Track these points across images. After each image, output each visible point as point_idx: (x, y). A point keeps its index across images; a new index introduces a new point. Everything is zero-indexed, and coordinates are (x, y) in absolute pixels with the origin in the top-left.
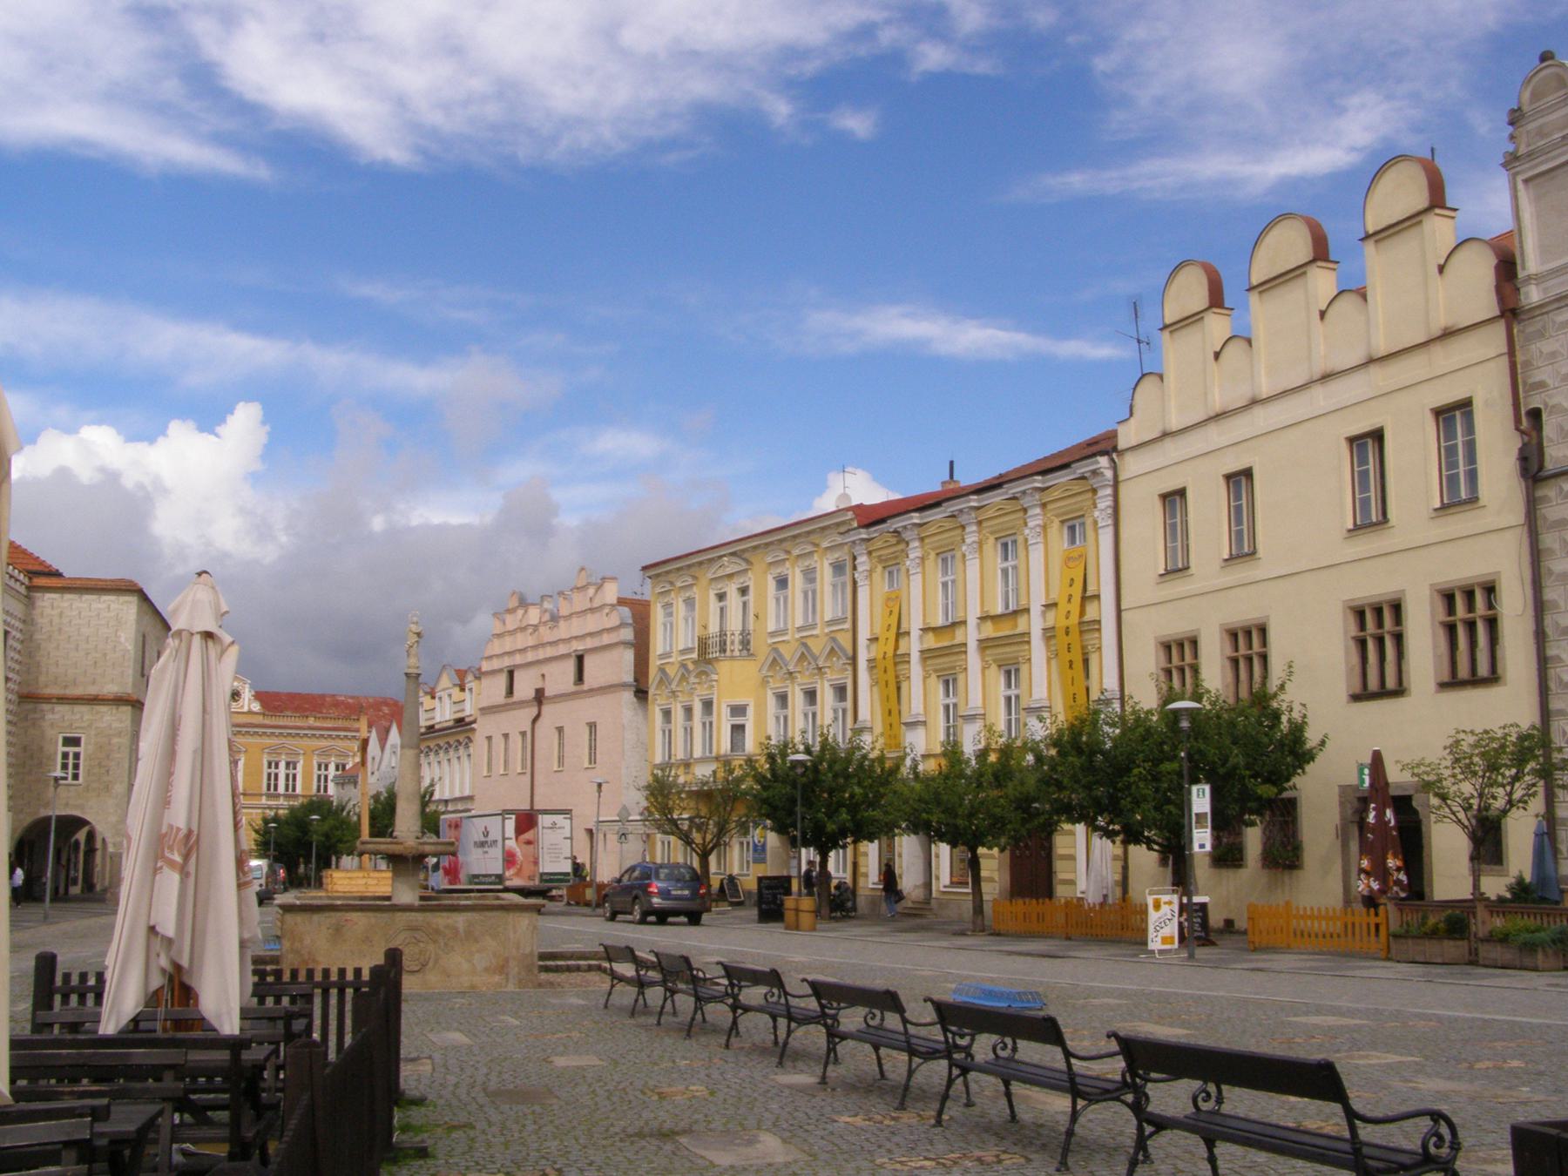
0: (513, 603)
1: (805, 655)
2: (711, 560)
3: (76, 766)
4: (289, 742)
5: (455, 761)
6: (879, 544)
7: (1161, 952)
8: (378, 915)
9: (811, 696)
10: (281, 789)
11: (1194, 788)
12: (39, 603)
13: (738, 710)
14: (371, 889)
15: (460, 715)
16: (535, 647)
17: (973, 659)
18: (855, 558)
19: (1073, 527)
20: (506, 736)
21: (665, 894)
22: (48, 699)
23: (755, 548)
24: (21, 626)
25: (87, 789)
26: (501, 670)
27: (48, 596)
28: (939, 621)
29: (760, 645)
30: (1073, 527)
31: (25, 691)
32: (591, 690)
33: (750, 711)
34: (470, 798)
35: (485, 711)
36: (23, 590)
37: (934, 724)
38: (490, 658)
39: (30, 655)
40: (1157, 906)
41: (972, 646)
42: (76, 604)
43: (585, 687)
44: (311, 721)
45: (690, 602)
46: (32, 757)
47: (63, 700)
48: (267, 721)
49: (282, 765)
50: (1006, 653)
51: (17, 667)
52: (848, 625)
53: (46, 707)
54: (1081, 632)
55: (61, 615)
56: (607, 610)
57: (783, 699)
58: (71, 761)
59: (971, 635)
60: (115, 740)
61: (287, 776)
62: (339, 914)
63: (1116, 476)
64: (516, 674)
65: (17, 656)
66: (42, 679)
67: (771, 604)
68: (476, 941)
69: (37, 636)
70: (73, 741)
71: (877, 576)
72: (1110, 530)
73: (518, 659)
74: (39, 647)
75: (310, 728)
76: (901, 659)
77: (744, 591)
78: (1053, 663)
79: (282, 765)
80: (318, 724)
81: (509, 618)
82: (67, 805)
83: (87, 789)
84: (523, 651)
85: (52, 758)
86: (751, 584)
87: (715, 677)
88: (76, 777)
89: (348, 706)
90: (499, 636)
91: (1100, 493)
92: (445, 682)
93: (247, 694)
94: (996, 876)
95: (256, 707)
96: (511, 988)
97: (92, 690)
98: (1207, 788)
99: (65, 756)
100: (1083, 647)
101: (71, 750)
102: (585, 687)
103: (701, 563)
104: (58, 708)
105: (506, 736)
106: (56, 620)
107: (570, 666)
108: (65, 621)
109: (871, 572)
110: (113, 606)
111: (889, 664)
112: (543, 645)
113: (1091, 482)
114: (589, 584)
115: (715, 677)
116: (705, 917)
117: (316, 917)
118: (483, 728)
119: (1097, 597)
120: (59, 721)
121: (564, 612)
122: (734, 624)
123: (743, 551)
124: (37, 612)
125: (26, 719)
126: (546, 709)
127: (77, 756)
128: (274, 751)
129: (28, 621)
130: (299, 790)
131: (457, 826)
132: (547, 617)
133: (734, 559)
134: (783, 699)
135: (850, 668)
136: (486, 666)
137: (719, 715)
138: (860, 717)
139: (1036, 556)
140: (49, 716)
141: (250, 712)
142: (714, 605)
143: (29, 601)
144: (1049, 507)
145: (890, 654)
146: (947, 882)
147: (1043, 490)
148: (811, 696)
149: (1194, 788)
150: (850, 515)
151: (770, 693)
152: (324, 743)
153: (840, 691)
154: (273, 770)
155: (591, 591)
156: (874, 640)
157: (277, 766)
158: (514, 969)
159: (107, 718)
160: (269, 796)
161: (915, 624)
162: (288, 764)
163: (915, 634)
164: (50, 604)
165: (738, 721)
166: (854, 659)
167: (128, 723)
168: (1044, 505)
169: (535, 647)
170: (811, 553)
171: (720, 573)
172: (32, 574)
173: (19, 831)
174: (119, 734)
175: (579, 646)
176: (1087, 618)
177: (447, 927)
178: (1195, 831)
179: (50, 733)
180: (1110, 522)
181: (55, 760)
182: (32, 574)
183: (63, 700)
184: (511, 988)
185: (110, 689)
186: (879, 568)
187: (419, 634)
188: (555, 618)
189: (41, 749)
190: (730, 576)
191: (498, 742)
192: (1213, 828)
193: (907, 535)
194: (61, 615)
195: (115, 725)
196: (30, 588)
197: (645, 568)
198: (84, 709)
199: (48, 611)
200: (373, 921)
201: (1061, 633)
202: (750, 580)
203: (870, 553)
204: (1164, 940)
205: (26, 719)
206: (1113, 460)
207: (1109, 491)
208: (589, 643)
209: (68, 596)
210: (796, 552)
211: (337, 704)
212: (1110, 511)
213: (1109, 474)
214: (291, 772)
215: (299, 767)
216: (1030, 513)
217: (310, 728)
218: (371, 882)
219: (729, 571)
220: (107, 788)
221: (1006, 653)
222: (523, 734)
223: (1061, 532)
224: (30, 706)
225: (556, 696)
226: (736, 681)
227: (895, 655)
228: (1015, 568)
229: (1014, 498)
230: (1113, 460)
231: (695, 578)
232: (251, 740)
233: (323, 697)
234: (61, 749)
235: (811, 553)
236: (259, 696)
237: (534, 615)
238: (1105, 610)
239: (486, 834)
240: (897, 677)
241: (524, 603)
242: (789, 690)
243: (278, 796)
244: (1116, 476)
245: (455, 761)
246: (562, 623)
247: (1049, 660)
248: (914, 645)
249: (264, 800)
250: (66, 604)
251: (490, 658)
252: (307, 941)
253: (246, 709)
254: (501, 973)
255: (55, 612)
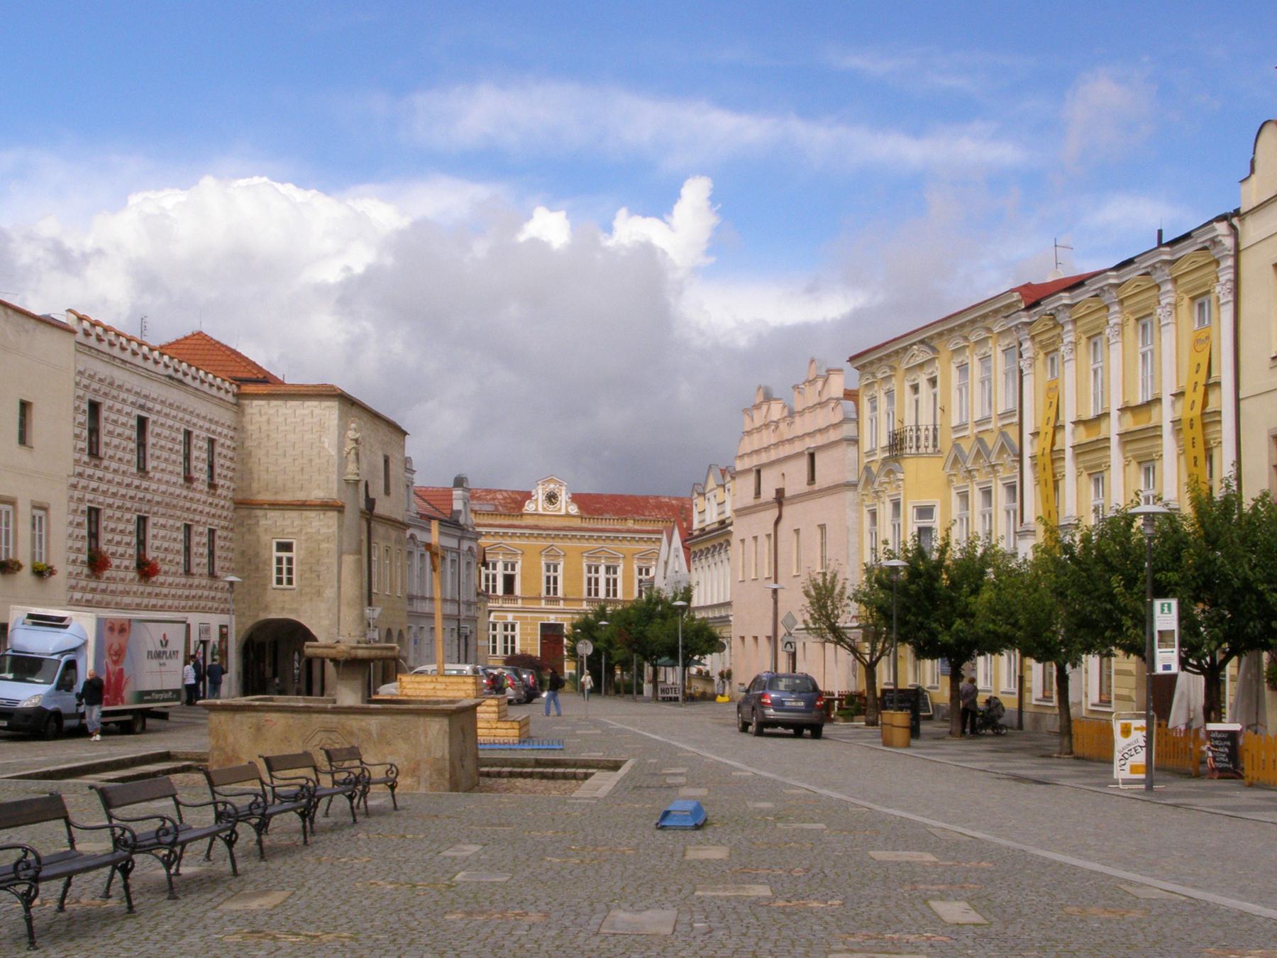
0: (760, 398)
1: (982, 451)
2: (905, 349)
3: (290, 571)
4: (608, 545)
5: (719, 564)
6: (1040, 328)
7: (1126, 782)
8: (295, 715)
9: (987, 493)
10: (602, 595)
11: (1158, 603)
12: (248, 410)
13: (924, 512)
14: (439, 693)
15: (722, 517)
16: (776, 445)
17: (1115, 455)
18: (1021, 345)
19: (1200, 299)
20: (755, 538)
21: (778, 705)
22: (260, 505)
23: (940, 334)
24: (231, 434)
25: (301, 593)
26: (749, 470)
27: (256, 403)
28: (1091, 414)
29: (945, 443)
30: (1200, 299)
31: (240, 497)
32: (820, 491)
33: (937, 512)
34: (728, 604)
35: (740, 512)
36: (230, 398)
37: (999, 526)
38: (742, 457)
39: (243, 462)
40: (1126, 732)
41: (1114, 441)
42: (282, 411)
43: (816, 487)
44: (630, 524)
45: (890, 394)
46: (250, 561)
47: (275, 506)
48: (585, 525)
49: (602, 569)
50: (1141, 444)
51: (230, 474)
52: (1016, 419)
53: (259, 513)
54: (1204, 425)
55: (268, 422)
56: (832, 405)
57: (964, 496)
58: (285, 566)
59: (1113, 428)
60: (324, 545)
61: (608, 580)
62: (261, 714)
63: (1237, 245)
64: (762, 474)
65: (228, 463)
66: (255, 485)
67: (955, 395)
68: (388, 743)
69: (248, 443)
70: (286, 547)
71: (1039, 363)
72: (1230, 307)
73: (764, 458)
74: (250, 454)
75: (628, 531)
76: (1056, 456)
77: (933, 382)
78: (1182, 458)
79: (602, 569)
80: (637, 527)
81: (756, 414)
82: (283, 609)
83: (301, 593)
84: (767, 449)
85: (267, 563)
86: (938, 374)
87: (901, 476)
88: (290, 581)
89: (671, 507)
90: (749, 433)
91: (1223, 265)
92: (711, 484)
93: (564, 497)
94: (1134, 695)
95: (574, 509)
96: (422, 790)
97: (301, 496)
98: (1174, 603)
99: (279, 560)
100: (1206, 442)
101: (285, 555)
102: (816, 487)
103: (897, 352)
104: (271, 514)
105: (755, 538)
106: (264, 427)
107: (804, 463)
108: (272, 427)
109: (1034, 358)
110: (316, 411)
111: (1047, 460)
112: (782, 443)
113: (1213, 252)
114: (818, 377)
115: (901, 476)
116: (827, 729)
117: (239, 717)
118: (739, 530)
119: (1218, 384)
120: (273, 526)
121: (798, 407)
122: (926, 420)
123: (931, 338)
124: (247, 419)
125: (242, 525)
126: (787, 510)
127: (290, 561)
128: (594, 554)
129: (238, 428)
130: (620, 596)
131: (122, 630)
132: (786, 413)
133: (923, 348)
134: (964, 496)
135: (1018, 465)
136: (739, 466)
137: (905, 516)
138: (1026, 520)
139: (1168, 339)
140: (262, 522)
141: (568, 515)
142: (908, 396)
143: (238, 408)
144: (1180, 282)
145: (1048, 451)
146: (1096, 700)
147: (1172, 262)
148: (987, 493)
149: (1158, 603)
150: (1016, 296)
151: (954, 493)
152: (644, 547)
153: (1011, 488)
154: (593, 575)
155: (820, 384)
156: (1035, 434)
157: (597, 571)
158: (425, 772)
159: (316, 523)
160: (549, 600)
161: (1068, 416)
162: (608, 568)
163: (1069, 427)
164: (260, 412)
165: (925, 523)
166: (1021, 455)
167: (335, 528)
168: (1175, 280)
169: (776, 445)
170: (986, 339)
171: (913, 363)
172: (240, 381)
173: (242, 633)
174: (327, 539)
175: (811, 443)
176: (1209, 409)
177: (360, 729)
178: (1157, 651)
179: (265, 538)
180: (1230, 298)
181: (270, 565)
182: (240, 381)
183: (275, 506)
184: (422, 790)
185: (317, 494)
186: (1041, 355)
187: (356, 441)
188: (792, 414)
189: (257, 555)
190: (921, 366)
191: (749, 541)
192: (1181, 645)
193: (1062, 317)
194: (268, 422)
195: (323, 530)
196: (239, 396)
197: (852, 359)
198: (294, 514)
199: (257, 418)
200: (291, 721)
201: (1185, 426)
202: (937, 370)
203: (1033, 338)
204: (1134, 769)
205: (242, 525)
206: (1232, 227)
207: (1230, 262)
208: (819, 440)
209: (274, 403)
210: (973, 338)
211: (659, 506)
212: (1230, 285)
213: (1229, 242)
214: (612, 576)
215: (620, 571)
216: (1163, 289)
217: (628, 531)
218: (439, 686)
219: (919, 360)
220: (319, 593)
221: (1141, 444)
222: (768, 536)
223: (1191, 311)
224: (244, 512)
225: (794, 497)
226: (922, 479)
227: (1052, 451)
228: (1152, 351)
229: (1147, 274)
230: (1232, 227)
231: (892, 368)
232: (569, 544)
233: (646, 499)
234: (276, 554)
235: (986, 339)
236: (576, 498)
237: (776, 411)
238: (1224, 400)
239: (165, 643)
240: (1054, 476)
241: (768, 398)
242: (993, 485)
243: (557, 600)
244: (1237, 245)
245: (719, 564)
246: (797, 419)
247: (1179, 455)
248: (1068, 439)
249: (543, 604)
250: (272, 411)
251: (742, 457)
252: (231, 739)
253: (563, 512)
254: (412, 776)
255: (264, 418)
